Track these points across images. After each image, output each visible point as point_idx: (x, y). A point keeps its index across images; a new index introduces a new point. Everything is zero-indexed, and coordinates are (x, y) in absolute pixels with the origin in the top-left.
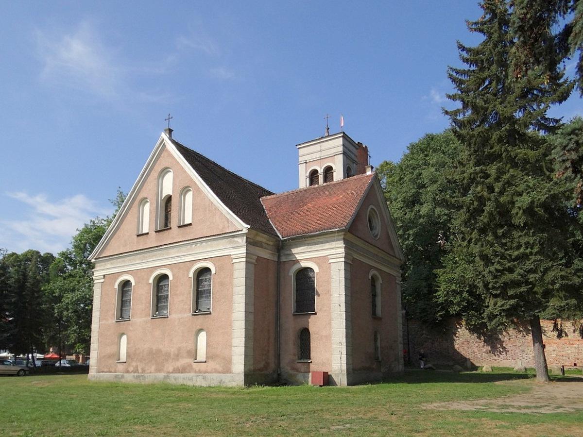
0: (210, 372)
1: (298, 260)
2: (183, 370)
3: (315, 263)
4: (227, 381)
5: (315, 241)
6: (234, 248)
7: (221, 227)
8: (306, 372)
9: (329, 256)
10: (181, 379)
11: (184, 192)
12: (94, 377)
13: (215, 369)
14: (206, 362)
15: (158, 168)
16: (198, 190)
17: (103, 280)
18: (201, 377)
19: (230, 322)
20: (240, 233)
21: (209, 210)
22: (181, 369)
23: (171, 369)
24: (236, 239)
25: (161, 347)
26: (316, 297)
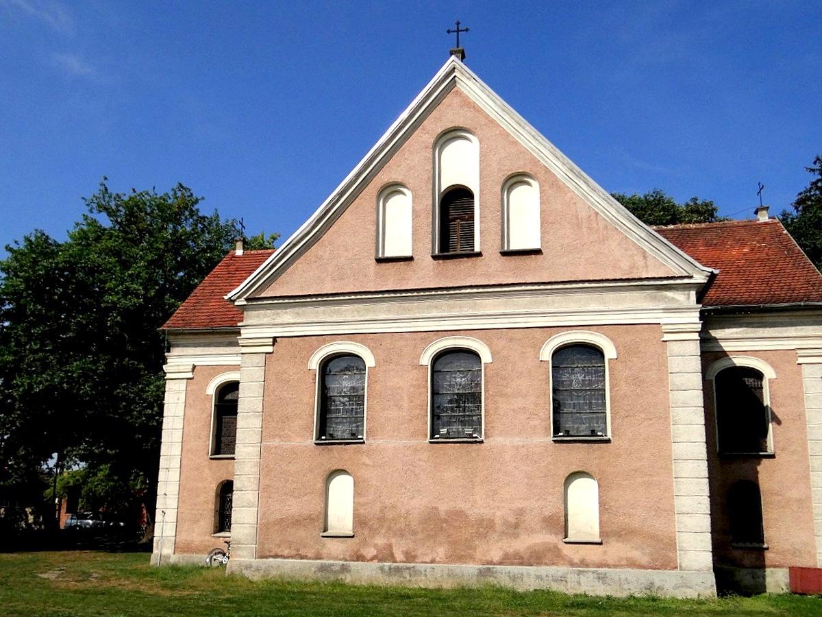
0: (615, 566)
1: (725, 352)
2: (536, 557)
3: (766, 360)
4: (667, 586)
5: (765, 320)
6: (666, 310)
7: (625, 264)
8: (756, 567)
9: (798, 351)
10: (530, 579)
11: (387, 192)
12: (249, 567)
13: (627, 559)
14: (601, 544)
15: (434, 126)
16: (551, 185)
17: (270, 349)
18: (591, 576)
19: (664, 461)
20: (686, 281)
21: (590, 228)
22: (526, 557)
23: (496, 555)
24: (670, 294)
25: (462, 506)
26: (770, 425)
